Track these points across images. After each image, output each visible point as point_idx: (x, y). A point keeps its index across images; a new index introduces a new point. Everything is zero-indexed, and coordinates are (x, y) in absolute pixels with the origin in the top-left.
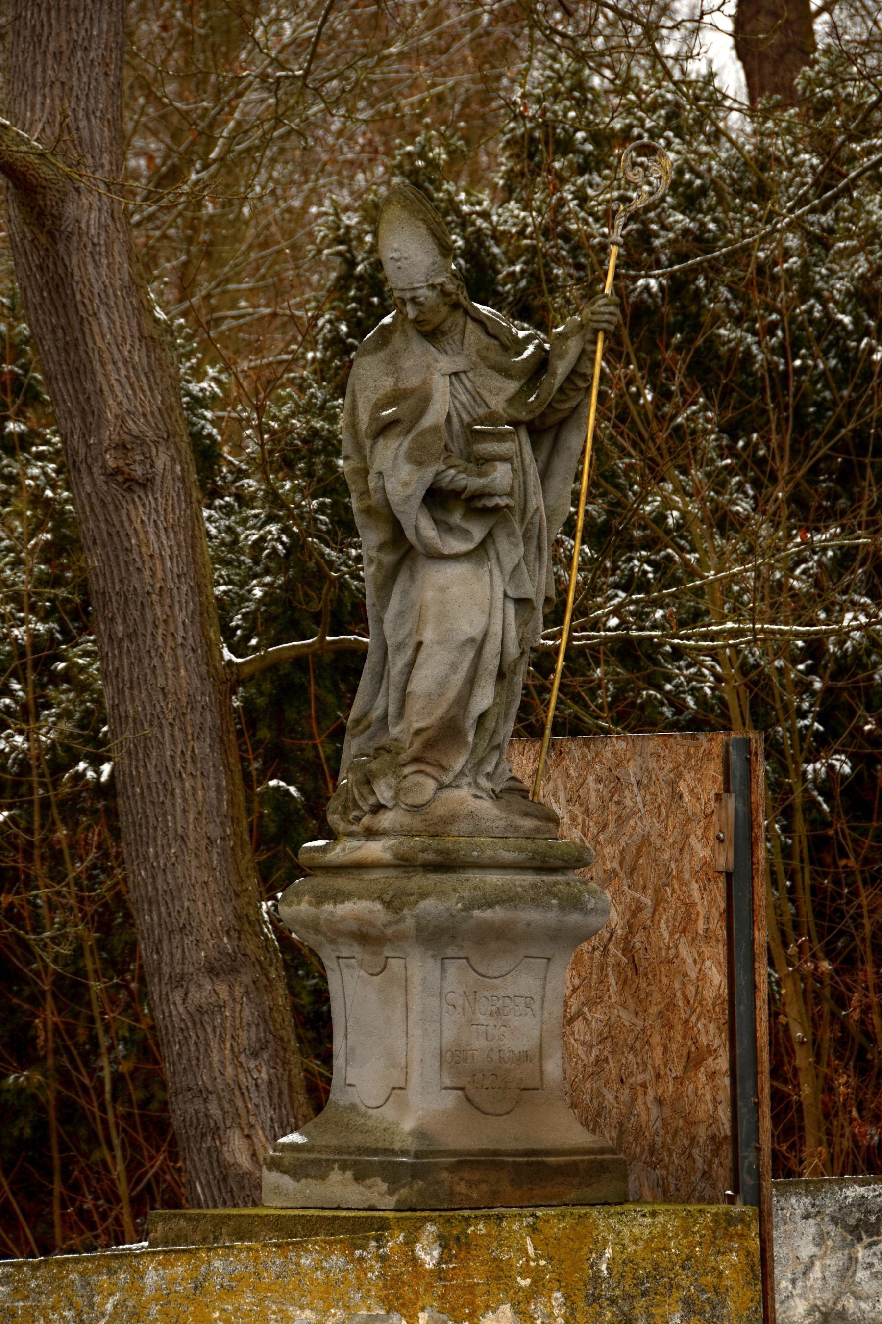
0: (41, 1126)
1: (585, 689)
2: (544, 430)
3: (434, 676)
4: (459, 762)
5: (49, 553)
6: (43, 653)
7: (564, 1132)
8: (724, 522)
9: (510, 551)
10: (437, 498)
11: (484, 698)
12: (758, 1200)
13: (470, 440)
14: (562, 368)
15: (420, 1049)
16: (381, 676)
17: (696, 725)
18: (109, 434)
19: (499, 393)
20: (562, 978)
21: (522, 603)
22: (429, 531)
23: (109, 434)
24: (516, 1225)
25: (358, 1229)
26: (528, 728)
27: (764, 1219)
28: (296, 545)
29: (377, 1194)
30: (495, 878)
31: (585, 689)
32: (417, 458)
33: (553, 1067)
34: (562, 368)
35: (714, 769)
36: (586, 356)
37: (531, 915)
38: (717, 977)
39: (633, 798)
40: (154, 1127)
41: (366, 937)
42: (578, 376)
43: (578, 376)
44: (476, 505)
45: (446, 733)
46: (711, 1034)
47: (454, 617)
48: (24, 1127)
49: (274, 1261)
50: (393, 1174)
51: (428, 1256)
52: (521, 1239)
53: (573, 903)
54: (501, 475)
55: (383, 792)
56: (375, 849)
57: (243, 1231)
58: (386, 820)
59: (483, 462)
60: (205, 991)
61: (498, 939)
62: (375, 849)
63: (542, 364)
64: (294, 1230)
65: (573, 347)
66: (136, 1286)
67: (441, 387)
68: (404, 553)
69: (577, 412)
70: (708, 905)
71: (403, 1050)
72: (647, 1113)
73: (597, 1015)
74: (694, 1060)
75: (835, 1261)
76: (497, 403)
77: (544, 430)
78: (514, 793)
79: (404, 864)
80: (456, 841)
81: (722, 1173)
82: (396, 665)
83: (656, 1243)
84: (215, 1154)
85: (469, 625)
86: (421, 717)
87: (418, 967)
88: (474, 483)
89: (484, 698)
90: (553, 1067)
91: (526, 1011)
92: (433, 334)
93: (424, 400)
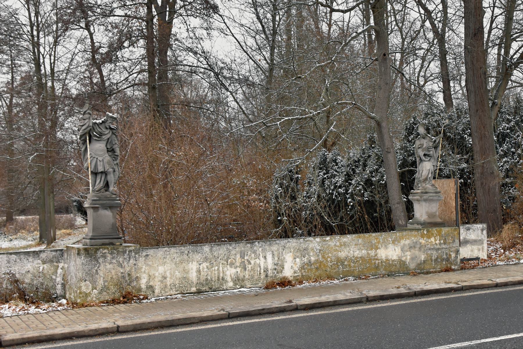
0: (378, 220)
1: (439, 174)
2: (436, 148)
3: (425, 173)
4: (427, 182)
5: (377, 159)
6: (377, 170)
7: (439, 220)
8: (450, 155)
9: (432, 160)
10: (425, 155)
11: (430, 175)
12: (458, 226)
13: (428, 149)
14: (437, 141)
15: (424, 212)
16: (419, 173)
17: (448, 177)
18: (386, 147)
19: (431, 144)
20: (438, 204)
21: (434, 166)
22: (424, 158)
23: (386, 147)
24: (434, 229)
25: (418, 230)
26: (434, 178)
27: (459, 229)
28: (404, 158)
29: (420, 227)
30: (431, 194)
31: (439, 174)
32: (423, 151)
33: (437, 213)
34: (437, 141)
35: (454, 183)
36: (440, 140)
37: (435, 198)
38: (454, 204)
39: (445, 186)
40: (390, 220)
41: (418, 200)
42: (439, 142)
43: (439, 142)
44: (429, 156)
45: (426, 179)
46: (454, 210)
47: (426, 168)
48: (376, 220)
49: (410, 233)
50: (421, 224)
51: (425, 232)
52: (434, 230)
53: (439, 197)
54: (431, 152)
55: (419, 185)
56: (419, 191)
57: (406, 230)
58: (420, 188)
59: (429, 151)
60: (397, 205)
61: (432, 200)
62: (419, 191)
63: (435, 141)
64: (411, 230)
65: (438, 139)
66: (396, 235)
67: (425, 143)
68: (421, 161)
69: (439, 146)
70: (453, 197)
71: (421, 211)
72: (447, 218)
73: (441, 208)
74: (452, 212)
75: (465, 233)
76: (431, 145)
77: (436, 148)
78: (433, 185)
79: (422, 193)
80: (427, 190)
81: (455, 224)
82: (421, 172)
83: (448, 231)
84: (398, 222)
85: (428, 168)
86: (423, 178)
87: (424, 204)
88: (428, 153)
89: (430, 175)
90: (437, 213)
91: (434, 208)
92: (424, 138)
93: (423, 145)
